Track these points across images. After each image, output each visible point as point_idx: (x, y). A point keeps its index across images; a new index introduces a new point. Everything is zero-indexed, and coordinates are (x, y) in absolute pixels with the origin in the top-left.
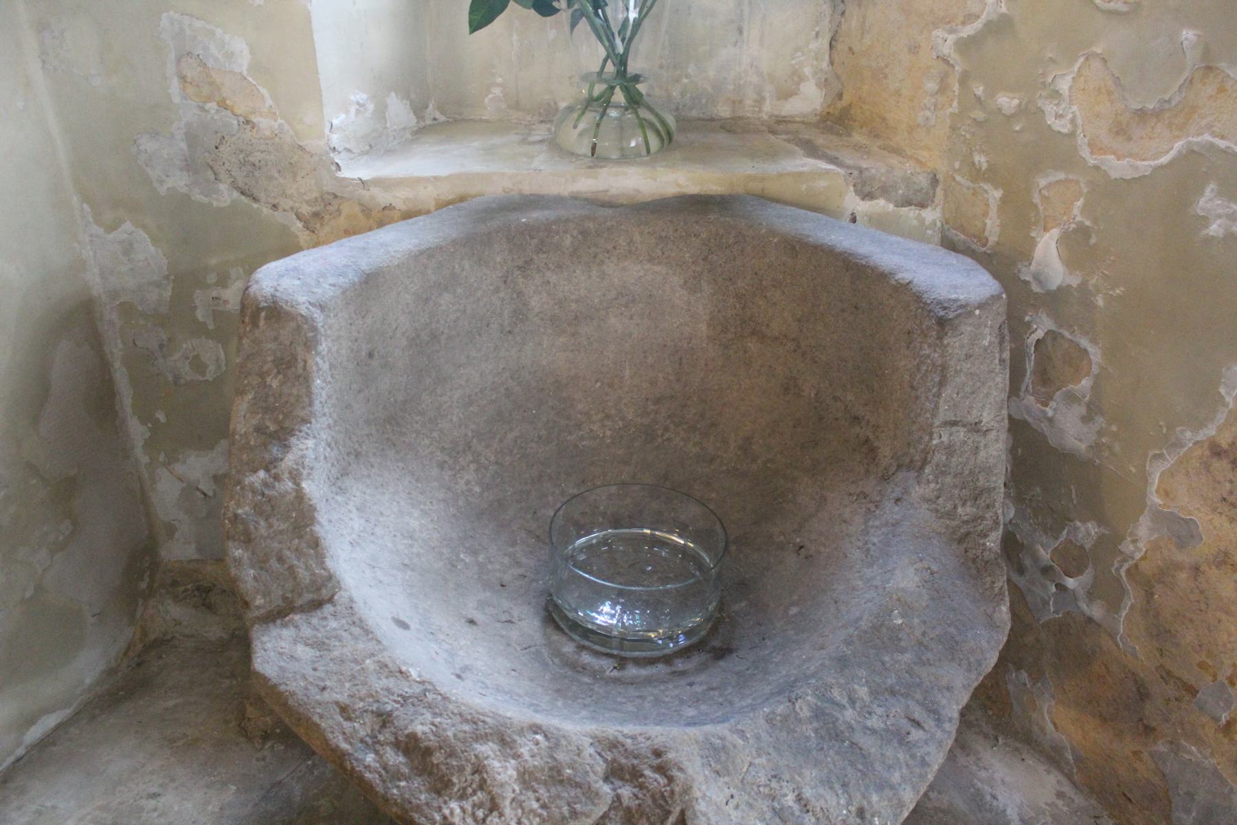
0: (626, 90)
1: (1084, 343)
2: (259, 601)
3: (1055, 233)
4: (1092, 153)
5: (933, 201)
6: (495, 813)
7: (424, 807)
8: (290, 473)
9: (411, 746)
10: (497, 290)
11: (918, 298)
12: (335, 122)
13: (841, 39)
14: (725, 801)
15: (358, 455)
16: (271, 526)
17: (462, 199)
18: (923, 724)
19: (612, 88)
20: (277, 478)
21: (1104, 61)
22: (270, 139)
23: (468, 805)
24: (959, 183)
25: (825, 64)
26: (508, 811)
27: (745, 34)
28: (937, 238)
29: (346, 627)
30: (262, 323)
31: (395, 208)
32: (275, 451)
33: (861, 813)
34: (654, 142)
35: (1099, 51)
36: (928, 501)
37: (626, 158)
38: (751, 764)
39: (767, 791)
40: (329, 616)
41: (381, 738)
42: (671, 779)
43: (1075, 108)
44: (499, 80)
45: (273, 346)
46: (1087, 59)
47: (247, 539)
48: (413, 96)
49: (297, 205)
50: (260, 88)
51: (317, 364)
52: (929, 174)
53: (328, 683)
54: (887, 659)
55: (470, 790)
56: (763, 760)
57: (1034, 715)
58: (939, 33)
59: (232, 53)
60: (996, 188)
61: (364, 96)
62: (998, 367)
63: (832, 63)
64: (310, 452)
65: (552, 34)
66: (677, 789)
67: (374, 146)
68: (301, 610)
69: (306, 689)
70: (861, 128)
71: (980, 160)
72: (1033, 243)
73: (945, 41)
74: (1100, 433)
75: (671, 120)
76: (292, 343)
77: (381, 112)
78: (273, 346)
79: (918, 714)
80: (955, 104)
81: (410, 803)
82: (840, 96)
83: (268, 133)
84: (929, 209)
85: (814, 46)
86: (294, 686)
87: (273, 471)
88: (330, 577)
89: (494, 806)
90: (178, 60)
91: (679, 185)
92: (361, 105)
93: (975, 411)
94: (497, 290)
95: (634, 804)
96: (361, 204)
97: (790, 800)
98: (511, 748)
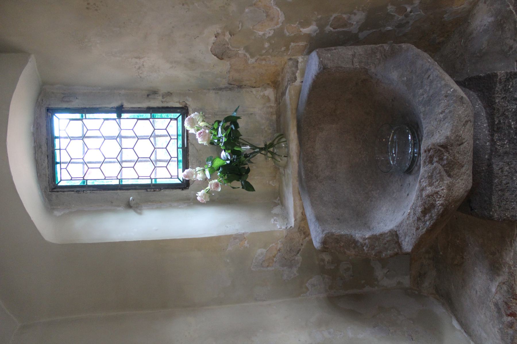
0: (269, 148)
1: (332, 18)
2: (396, 250)
3: (301, 29)
4: (279, 24)
5: (296, 59)
6: (439, 193)
7: (438, 210)
8: (364, 240)
9: (425, 212)
10: (323, 185)
11: (319, 74)
12: (279, 227)
13: (252, 85)
14: (439, 134)
15: (366, 224)
16: (377, 246)
17: (299, 193)
18: (429, 75)
19: (269, 152)
20: (365, 244)
21: (254, 26)
22: (283, 245)
23: (437, 199)
24: (290, 53)
25: (260, 89)
26: (438, 190)
27: (252, 112)
28: (307, 57)
29: (401, 228)
30: (327, 246)
31: (302, 212)
32: (359, 244)
33: (446, 96)
34: (283, 140)
35: (252, 27)
36: (375, 67)
37: (287, 147)
38: (432, 126)
39: (439, 122)
40: (399, 232)
41: (423, 220)
42: (431, 149)
43: (267, 30)
44: (268, 182)
45: (333, 244)
46: (254, 29)
47: (380, 252)
48: (272, 206)
49: (301, 238)
50: (270, 247)
51: (338, 233)
52: (288, 61)
53: (412, 233)
54: (414, 83)
55: (434, 199)
56: (432, 122)
57: (459, 11)
58: (249, 62)
59: (261, 253)
60: (291, 44)
61: (272, 219)
62: (337, 50)
63: (259, 87)
64: (359, 235)
65: (254, 167)
66: (433, 147)
67: (285, 217)
68: (398, 239)
69: (414, 238)
70: (277, 78)
71: (283, 49)
72: (305, 34)
73: (251, 61)
74: (358, 10)
75: (276, 135)
76: (332, 239)
77: (277, 215)
78: (333, 244)
79: (427, 76)
80: (268, 56)
81: (437, 214)
82: (268, 84)
83: (282, 245)
84: (298, 60)
85: (254, 92)
86: (413, 241)
87: (364, 245)
88: (390, 231)
89: (437, 193)
90: (263, 267)
91: (294, 133)
92: (275, 220)
93: (349, 57)
94: (323, 185)
95: (438, 158)
96: (301, 221)
97: (441, 116)
98: (424, 188)
